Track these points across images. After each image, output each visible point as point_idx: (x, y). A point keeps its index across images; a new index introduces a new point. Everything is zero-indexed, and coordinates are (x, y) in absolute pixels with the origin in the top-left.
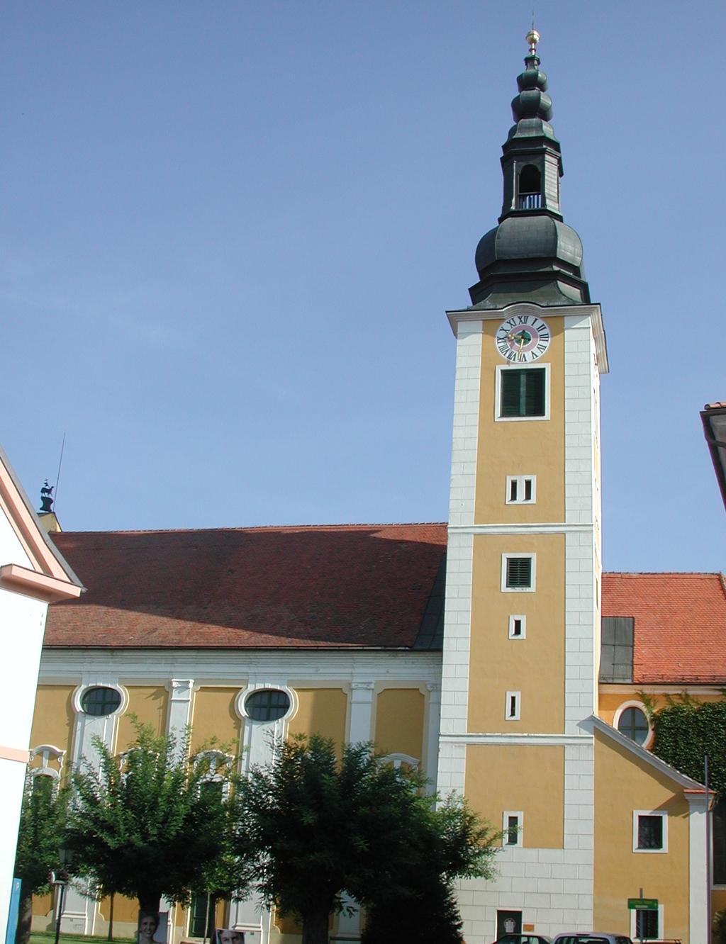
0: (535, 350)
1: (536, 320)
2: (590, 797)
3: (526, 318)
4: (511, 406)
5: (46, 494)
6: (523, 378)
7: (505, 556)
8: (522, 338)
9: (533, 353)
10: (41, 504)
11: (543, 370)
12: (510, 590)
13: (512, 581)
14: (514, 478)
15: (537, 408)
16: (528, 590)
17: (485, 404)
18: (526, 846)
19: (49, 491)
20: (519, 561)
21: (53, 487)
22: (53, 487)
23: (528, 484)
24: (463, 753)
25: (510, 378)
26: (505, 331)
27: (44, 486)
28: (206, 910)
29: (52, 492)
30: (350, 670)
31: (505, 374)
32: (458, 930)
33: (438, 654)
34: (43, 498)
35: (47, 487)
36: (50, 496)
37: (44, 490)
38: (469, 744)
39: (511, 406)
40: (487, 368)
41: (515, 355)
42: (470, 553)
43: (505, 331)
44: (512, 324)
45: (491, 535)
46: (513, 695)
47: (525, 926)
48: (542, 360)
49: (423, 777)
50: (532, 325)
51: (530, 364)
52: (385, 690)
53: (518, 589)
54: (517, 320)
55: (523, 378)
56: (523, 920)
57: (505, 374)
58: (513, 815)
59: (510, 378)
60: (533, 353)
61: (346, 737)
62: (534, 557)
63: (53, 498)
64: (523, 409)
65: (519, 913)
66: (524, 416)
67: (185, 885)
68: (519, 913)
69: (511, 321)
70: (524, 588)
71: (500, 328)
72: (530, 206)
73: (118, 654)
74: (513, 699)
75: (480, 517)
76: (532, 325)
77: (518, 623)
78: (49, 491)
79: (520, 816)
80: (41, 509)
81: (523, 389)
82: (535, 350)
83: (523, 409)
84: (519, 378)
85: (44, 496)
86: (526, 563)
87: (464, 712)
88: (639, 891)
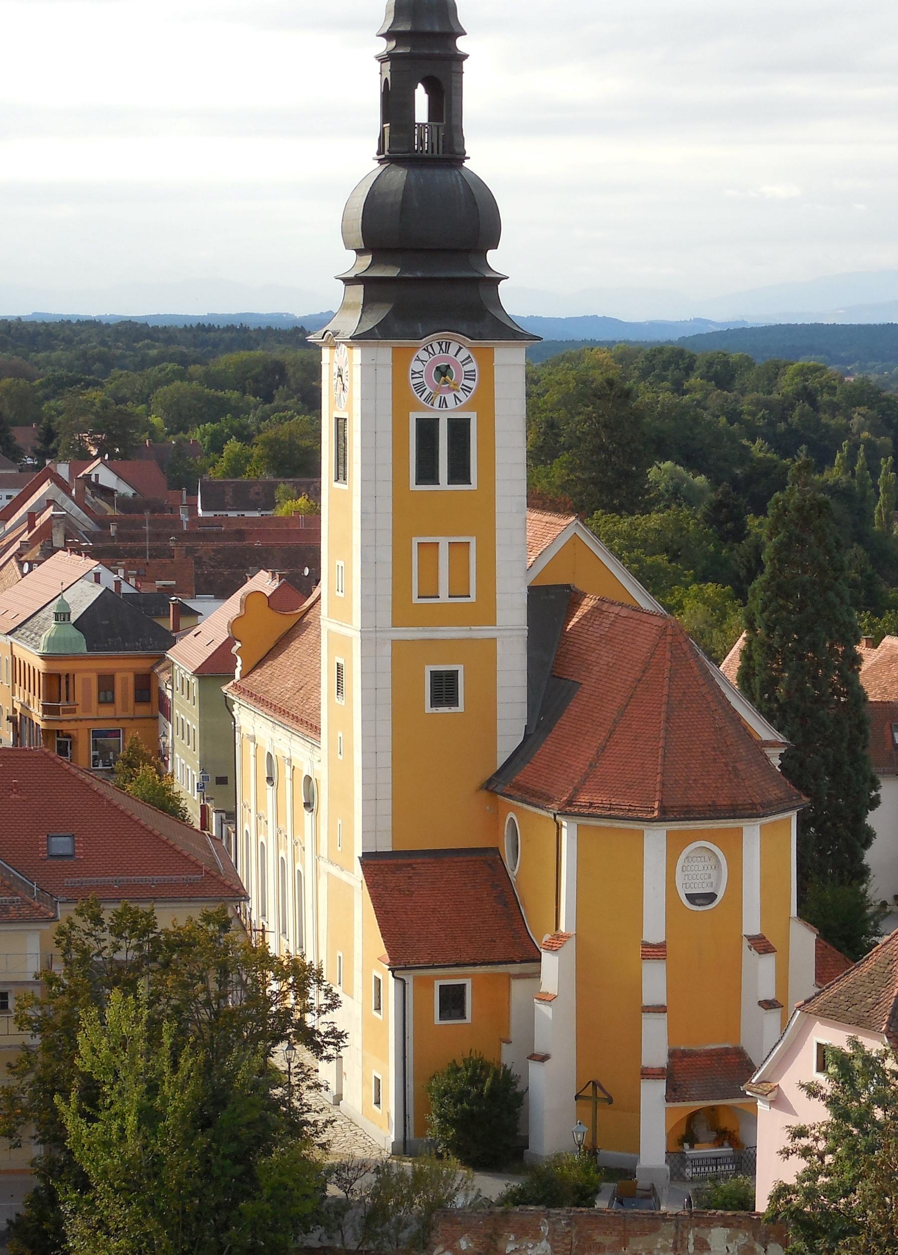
1: (460, 348)
3: (448, 345)
7: (428, 669)
8: (445, 376)
11: (468, 420)
12: (434, 710)
16: (454, 709)
20: (444, 673)
26: (422, 361)
28: (35, 533)
32: (14, 1221)
33: (538, 964)
43: (422, 361)
44: (430, 353)
48: (467, 407)
50: (456, 356)
54: (436, 348)
61: (386, 375)
67: (238, 1205)
69: (429, 347)
71: (411, 372)
72: (438, 153)
76: (456, 356)
86: (436, 701)
88: (386, 1114)
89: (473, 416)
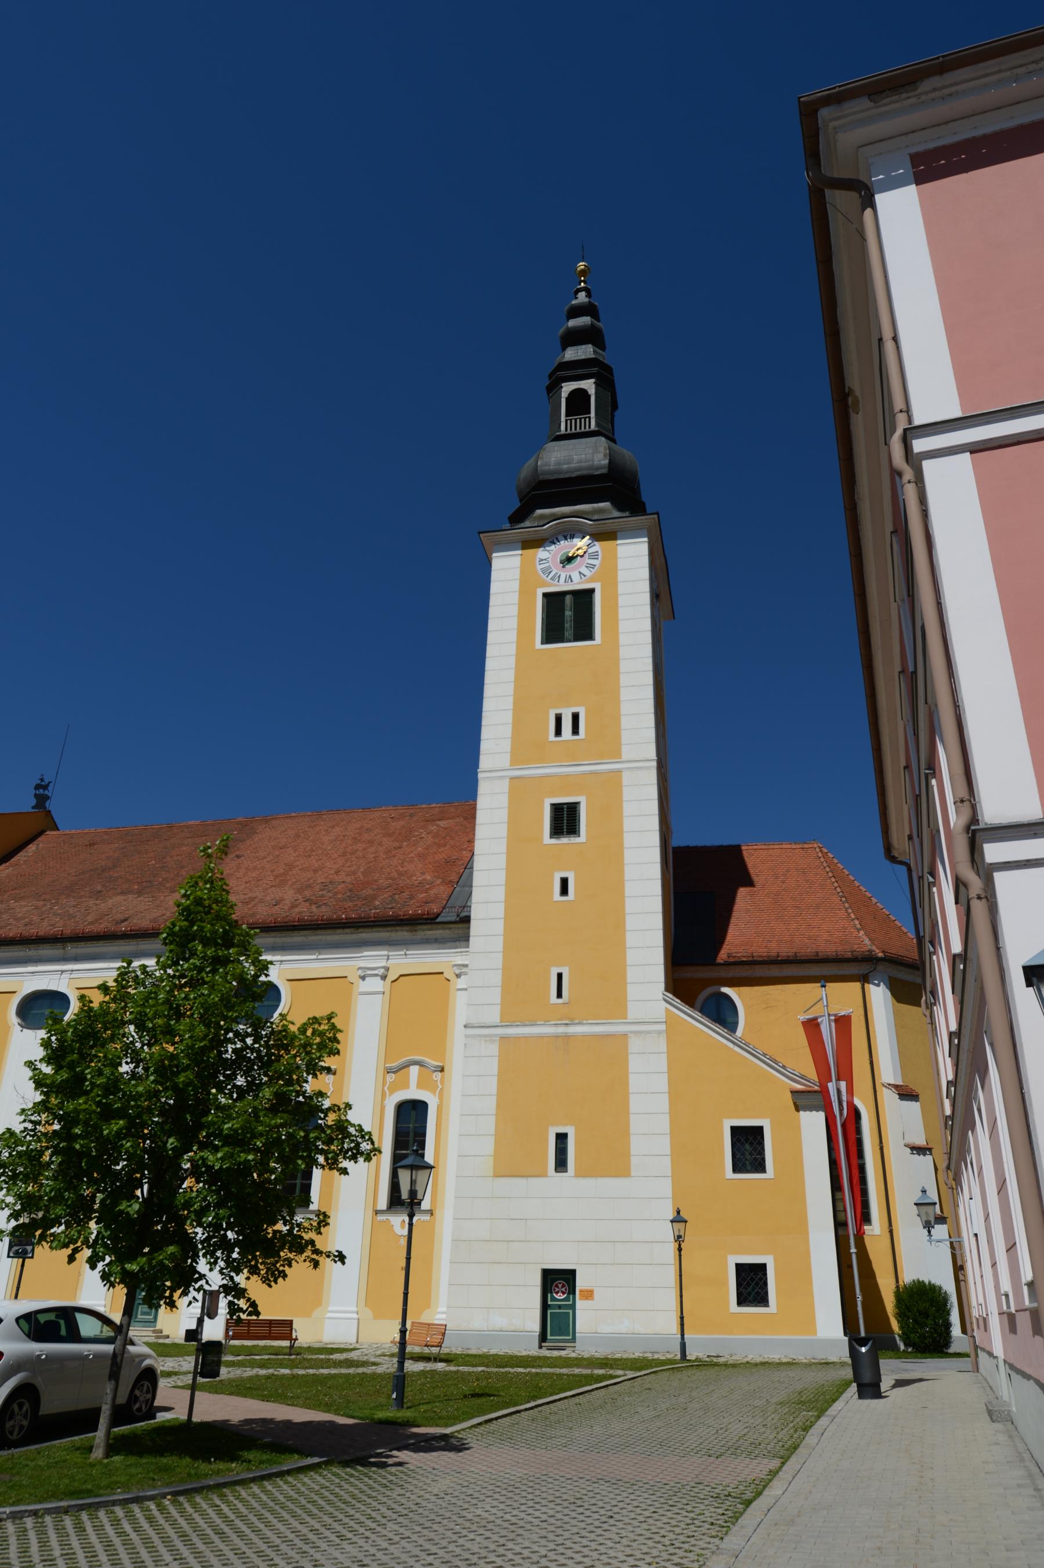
0: (584, 570)
2: (663, 1103)
4: (553, 633)
5: (41, 791)
6: (568, 599)
9: (580, 573)
10: (34, 802)
12: (554, 841)
13: (557, 830)
14: (558, 711)
15: (584, 631)
17: (523, 632)
18: (577, 1175)
19: (45, 787)
21: (50, 782)
22: (50, 782)
23: (576, 717)
24: (494, 1049)
25: (553, 600)
27: (39, 782)
29: (50, 788)
30: (386, 953)
31: (546, 595)
33: (465, 925)
34: (36, 796)
35: (43, 783)
36: (46, 792)
37: (38, 787)
38: (503, 1038)
39: (553, 633)
40: (525, 592)
41: (559, 576)
42: (504, 800)
45: (529, 777)
46: (560, 971)
47: (581, 1291)
48: (592, 580)
49: (281, 1480)
51: (578, 584)
52: (401, 976)
53: (564, 840)
55: (568, 599)
56: (577, 1284)
57: (546, 595)
58: (562, 1130)
59: (553, 600)
60: (580, 573)
62: (582, 800)
63: (49, 794)
64: (569, 633)
65: (572, 1273)
66: (570, 641)
68: (572, 1273)
70: (572, 839)
71: (538, 560)
73: (366, 953)
74: (560, 976)
75: (518, 758)
77: (564, 882)
78: (45, 787)
79: (570, 1130)
80: (33, 808)
81: (568, 613)
82: (584, 570)
83: (569, 633)
84: (564, 601)
85: (37, 792)
87: (506, 745)
89: (597, 586)
